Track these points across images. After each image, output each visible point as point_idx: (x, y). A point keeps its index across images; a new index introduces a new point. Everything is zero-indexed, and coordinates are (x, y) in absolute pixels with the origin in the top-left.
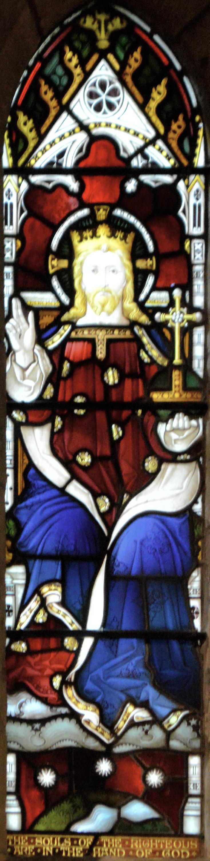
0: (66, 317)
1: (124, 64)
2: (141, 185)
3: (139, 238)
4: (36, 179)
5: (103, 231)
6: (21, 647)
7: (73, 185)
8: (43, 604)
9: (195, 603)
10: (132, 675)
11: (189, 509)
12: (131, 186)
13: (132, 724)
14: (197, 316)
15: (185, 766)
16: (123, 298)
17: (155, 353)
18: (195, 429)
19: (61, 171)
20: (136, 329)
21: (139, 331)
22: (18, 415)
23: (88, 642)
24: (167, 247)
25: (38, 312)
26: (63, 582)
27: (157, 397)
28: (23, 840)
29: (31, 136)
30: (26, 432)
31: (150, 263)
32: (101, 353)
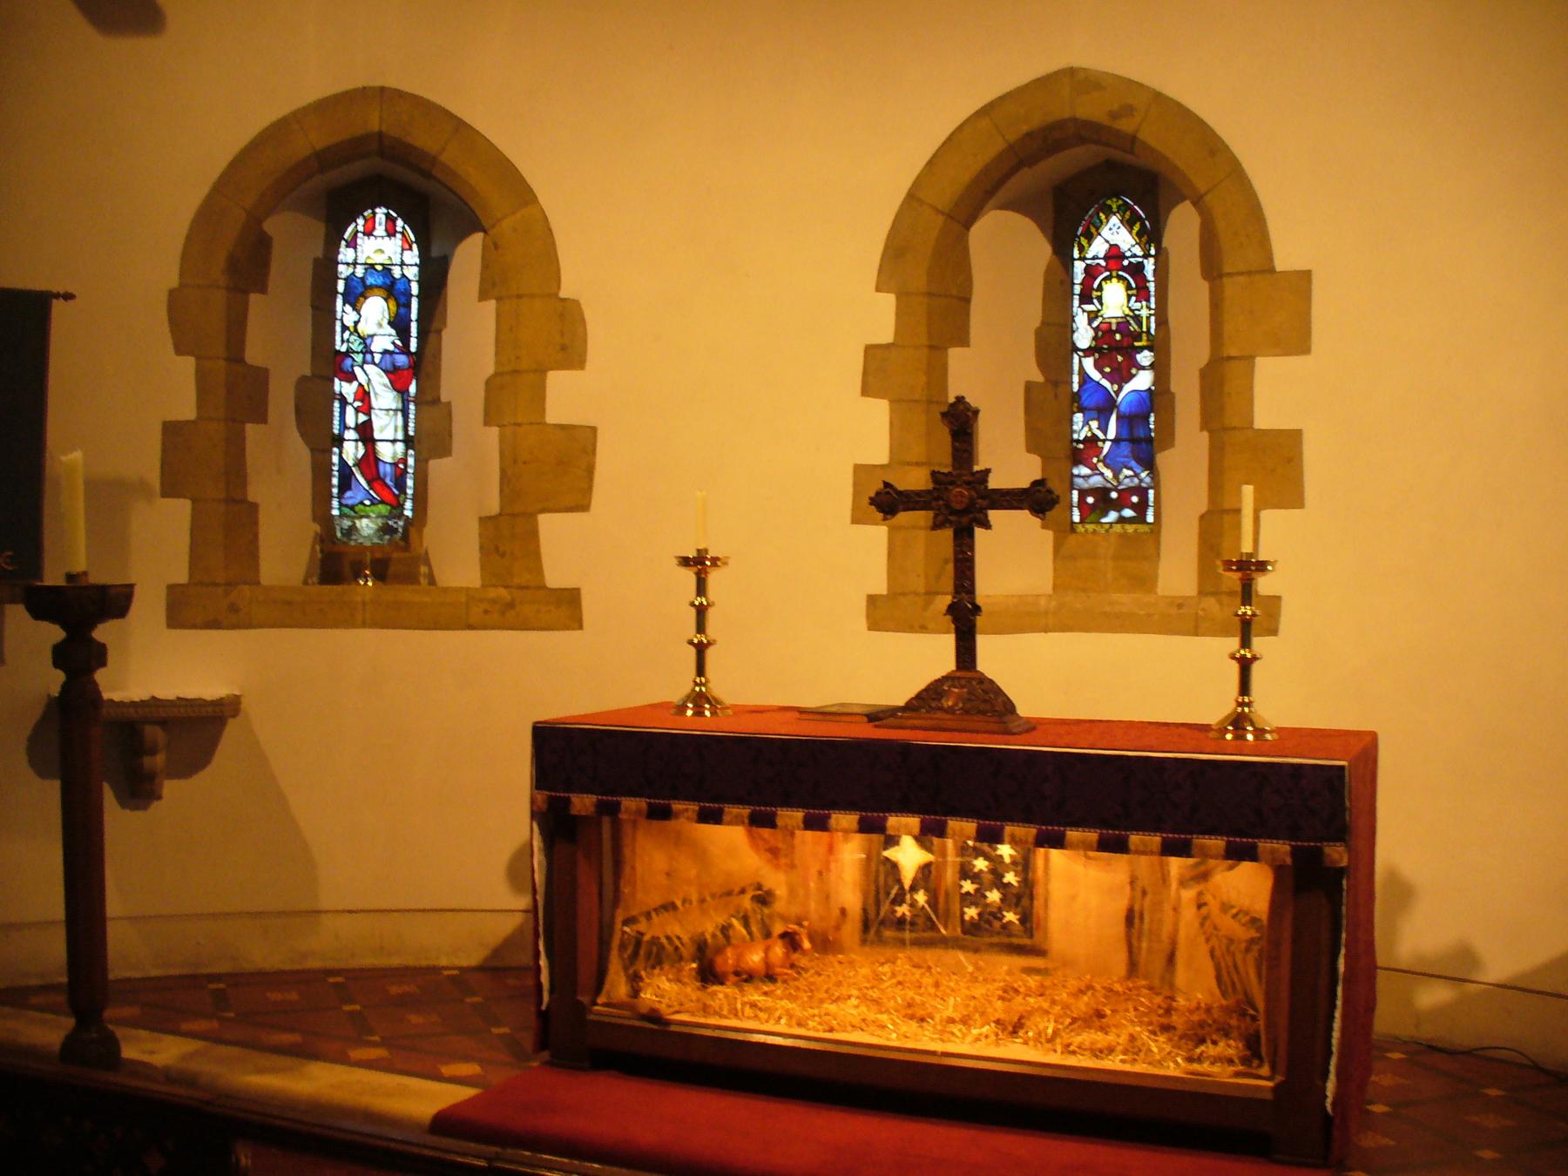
0: (1100, 314)
1: (1123, 217)
2: (1130, 263)
3: (1129, 284)
4: (1089, 262)
5: (1114, 280)
6: (1081, 446)
7: (1103, 263)
8: (1090, 429)
9: (1152, 427)
10: (1126, 457)
11: (1150, 389)
12: (1126, 263)
13: (1126, 477)
14: (1152, 312)
15: (1147, 493)
16: (1123, 305)
17: (1136, 327)
18: (1205, 198)
19: (1098, 258)
20: (1128, 318)
21: (1128, 318)
22: (1081, 353)
23: (1108, 444)
24: (1141, 285)
25: (1089, 313)
26: (1098, 419)
27: (1136, 344)
28: (1080, 526)
29: (1104, 221)
30: (1083, 359)
31: (1134, 292)
32: (1114, 327)
